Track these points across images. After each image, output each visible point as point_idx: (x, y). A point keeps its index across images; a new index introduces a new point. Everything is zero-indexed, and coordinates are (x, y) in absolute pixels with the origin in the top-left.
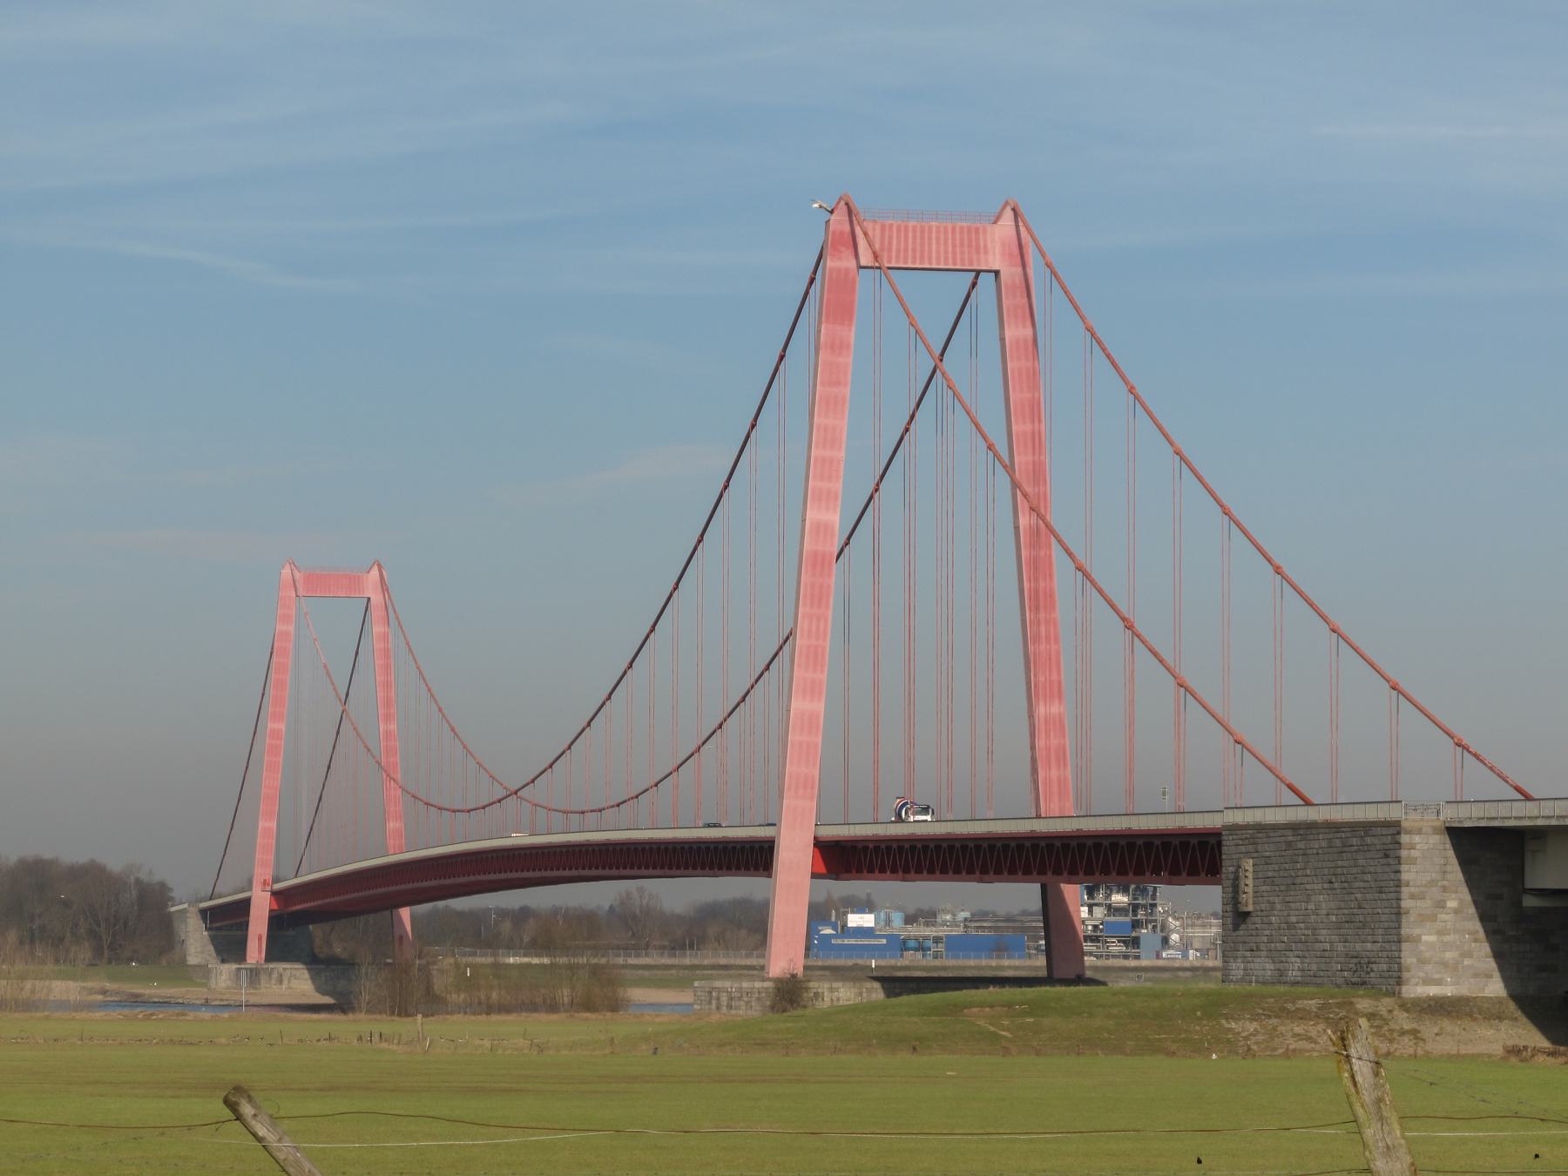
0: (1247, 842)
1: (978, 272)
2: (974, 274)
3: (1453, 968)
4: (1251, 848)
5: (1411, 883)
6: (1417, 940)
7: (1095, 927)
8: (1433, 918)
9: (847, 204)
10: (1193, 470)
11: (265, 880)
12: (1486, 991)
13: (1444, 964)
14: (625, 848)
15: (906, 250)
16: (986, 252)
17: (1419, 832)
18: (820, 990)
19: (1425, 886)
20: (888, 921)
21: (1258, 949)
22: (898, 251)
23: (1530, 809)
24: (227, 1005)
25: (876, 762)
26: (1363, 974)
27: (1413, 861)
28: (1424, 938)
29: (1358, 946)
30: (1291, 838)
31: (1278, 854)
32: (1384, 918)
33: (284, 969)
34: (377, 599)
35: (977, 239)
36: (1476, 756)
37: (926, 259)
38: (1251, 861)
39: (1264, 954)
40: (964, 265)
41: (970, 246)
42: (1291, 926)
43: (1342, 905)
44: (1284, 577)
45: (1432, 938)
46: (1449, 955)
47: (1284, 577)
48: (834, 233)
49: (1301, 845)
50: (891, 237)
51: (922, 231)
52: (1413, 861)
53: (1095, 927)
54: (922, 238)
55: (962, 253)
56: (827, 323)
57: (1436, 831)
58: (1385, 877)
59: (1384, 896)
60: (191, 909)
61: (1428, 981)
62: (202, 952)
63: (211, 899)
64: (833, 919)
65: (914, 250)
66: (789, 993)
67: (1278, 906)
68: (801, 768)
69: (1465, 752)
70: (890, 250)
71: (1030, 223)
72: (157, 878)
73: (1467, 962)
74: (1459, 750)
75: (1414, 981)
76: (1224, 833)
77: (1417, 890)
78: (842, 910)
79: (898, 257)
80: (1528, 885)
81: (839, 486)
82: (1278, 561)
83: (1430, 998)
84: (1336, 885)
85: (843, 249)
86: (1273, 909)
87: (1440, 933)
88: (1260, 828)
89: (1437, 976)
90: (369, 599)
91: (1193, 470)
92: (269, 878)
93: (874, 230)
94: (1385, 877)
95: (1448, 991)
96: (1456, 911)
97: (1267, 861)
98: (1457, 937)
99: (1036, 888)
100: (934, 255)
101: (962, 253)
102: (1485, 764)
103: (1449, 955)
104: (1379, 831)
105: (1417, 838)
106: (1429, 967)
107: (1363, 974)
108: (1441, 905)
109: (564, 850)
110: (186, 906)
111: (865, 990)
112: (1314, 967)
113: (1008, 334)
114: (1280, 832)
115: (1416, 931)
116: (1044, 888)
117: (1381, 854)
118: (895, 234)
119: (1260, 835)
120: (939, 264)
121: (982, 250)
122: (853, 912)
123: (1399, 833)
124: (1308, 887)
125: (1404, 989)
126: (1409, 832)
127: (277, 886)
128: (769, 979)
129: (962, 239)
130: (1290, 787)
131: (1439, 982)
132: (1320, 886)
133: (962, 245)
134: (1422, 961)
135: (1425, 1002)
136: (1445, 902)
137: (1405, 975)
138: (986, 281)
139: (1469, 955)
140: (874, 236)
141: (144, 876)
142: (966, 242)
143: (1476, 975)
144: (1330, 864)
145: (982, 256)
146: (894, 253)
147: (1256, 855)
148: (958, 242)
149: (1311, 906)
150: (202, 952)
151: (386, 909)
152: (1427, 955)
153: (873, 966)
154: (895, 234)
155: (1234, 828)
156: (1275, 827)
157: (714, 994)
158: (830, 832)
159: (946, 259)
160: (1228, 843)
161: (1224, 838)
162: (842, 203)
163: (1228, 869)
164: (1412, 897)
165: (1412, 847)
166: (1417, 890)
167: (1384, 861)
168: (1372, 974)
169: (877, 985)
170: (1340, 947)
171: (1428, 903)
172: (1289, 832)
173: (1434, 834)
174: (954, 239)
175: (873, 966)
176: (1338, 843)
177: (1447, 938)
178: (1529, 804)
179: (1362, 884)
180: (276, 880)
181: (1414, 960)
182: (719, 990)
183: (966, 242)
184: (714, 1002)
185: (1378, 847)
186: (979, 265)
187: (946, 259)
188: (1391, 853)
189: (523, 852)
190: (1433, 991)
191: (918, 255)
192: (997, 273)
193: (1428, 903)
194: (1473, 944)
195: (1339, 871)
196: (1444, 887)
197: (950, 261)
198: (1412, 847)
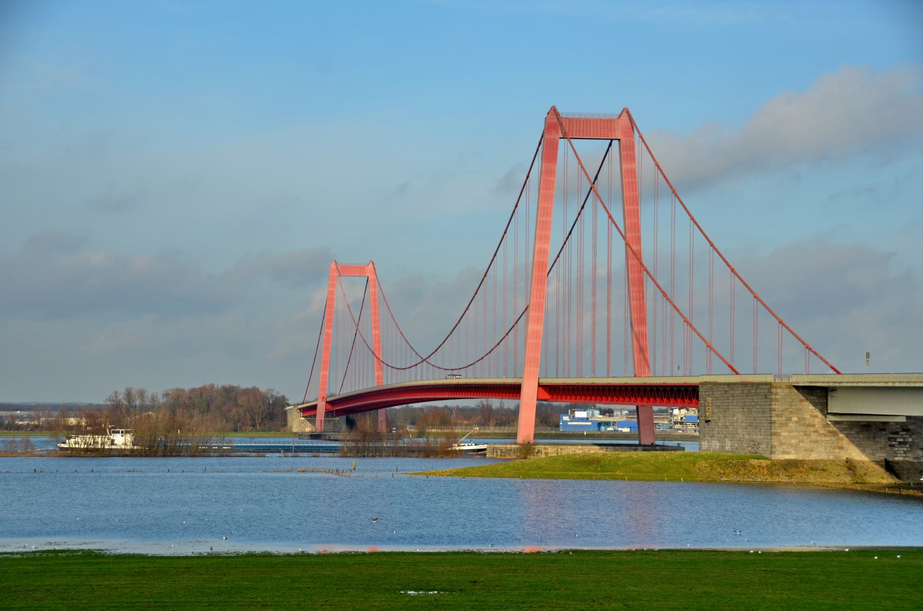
0: (709, 390)
1: (612, 140)
2: (610, 141)
3: (796, 447)
4: (711, 393)
5: (776, 410)
6: (778, 435)
7: (682, 418)
8: (786, 425)
9: (554, 110)
10: (699, 227)
11: (323, 397)
12: (810, 457)
13: (792, 445)
14: (462, 386)
15: (580, 130)
16: (614, 131)
17: (780, 388)
18: (540, 449)
19: (782, 411)
20: (593, 415)
21: (713, 436)
22: (576, 131)
23: (838, 378)
26: (756, 449)
28: (782, 434)
29: (754, 437)
30: (726, 389)
31: (721, 395)
32: (765, 425)
33: (332, 435)
34: (371, 277)
35: (611, 126)
36: (815, 353)
37: (578, 134)
38: (710, 399)
39: (716, 439)
40: (593, 136)
42: (726, 427)
43: (748, 418)
44: (736, 274)
45: (786, 434)
46: (793, 441)
47: (736, 274)
48: (548, 123)
49: (731, 392)
50: (573, 125)
52: (777, 400)
53: (682, 418)
54: (587, 125)
55: (604, 131)
56: (545, 162)
58: (766, 407)
59: (764, 415)
60: (295, 409)
61: (784, 453)
62: (299, 427)
63: (303, 404)
64: (569, 413)
65: (583, 131)
66: (527, 449)
67: (722, 418)
69: (810, 351)
70: (573, 131)
72: (280, 395)
73: (801, 444)
74: (807, 350)
75: (777, 452)
76: (700, 386)
77: (779, 412)
78: (573, 410)
79: (576, 133)
80: (829, 412)
82: (733, 266)
83: (786, 460)
84: (745, 410)
85: (552, 130)
86: (719, 419)
87: (789, 432)
88: (715, 384)
89: (789, 450)
90: (368, 277)
91: (699, 227)
93: (566, 122)
94: (766, 407)
95: (792, 457)
96: (796, 422)
97: (717, 399)
98: (797, 433)
100: (592, 132)
101: (604, 131)
103: (793, 441)
104: (763, 387)
105: (779, 390)
106: (784, 447)
107: (756, 449)
108: (789, 419)
109: (441, 387)
110: (292, 407)
111: (559, 449)
112: (736, 445)
113: (624, 167)
114: (722, 386)
115: (779, 431)
117: (764, 397)
118: (575, 123)
119: (714, 387)
120: (583, 136)
121: (613, 130)
122: (577, 411)
123: (771, 388)
124: (734, 410)
126: (776, 388)
128: (519, 444)
129: (604, 126)
131: (788, 453)
132: (739, 410)
133: (604, 128)
134: (781, 444)
135: (782, 461)
136: (791, 418)
138: (615, 143)
139: (803, 441)
140: (566, 124)
141: (275, 393)
142: (606, 127)
143: (806, 450)
144: (743, 401)
145: (613, 133)
146: (574, 132)
147: (712, 396)
148: (602, 127)
149: (735, 419)
150: (299, 427)
151: (374, 409)
152: (784, 441)
153: (585, 434)
154: (575, 123)
155: (706, 383)
156: (721, 384)
157: (495, 450)
158: (545, 381)
159: (597, 134)
160: (701, 390)
161: (700, 388)
163: (701, 401)
164: (777, 416)
165: (777, 394)
166: (779, 412)
167: (765, 400)
168: (760, 449)
170: (747, 437)
171: (784, 419)
172: (726, 386)
173: (786, 388)
174: (600, 126)
175: (585, 434)
176: (746, 392)
177: (792, 434)
178: (839, 376)
179: (756, 410)
181: (778, 443)
182: (497, 449)
183: (606, 127)
184: (495, 454)
185: (762, 394)
186: (611, 137)
187: (597, 134)
188: (768, 397)
189: (429, 387)
190: (787, 457)
191: (585, 132)
192: (619, 140)
193: (784, 419)
194: (804, 437)
195: (746, 404)
196: (791, 412)
197: (599, 135)
198: (777, 394)
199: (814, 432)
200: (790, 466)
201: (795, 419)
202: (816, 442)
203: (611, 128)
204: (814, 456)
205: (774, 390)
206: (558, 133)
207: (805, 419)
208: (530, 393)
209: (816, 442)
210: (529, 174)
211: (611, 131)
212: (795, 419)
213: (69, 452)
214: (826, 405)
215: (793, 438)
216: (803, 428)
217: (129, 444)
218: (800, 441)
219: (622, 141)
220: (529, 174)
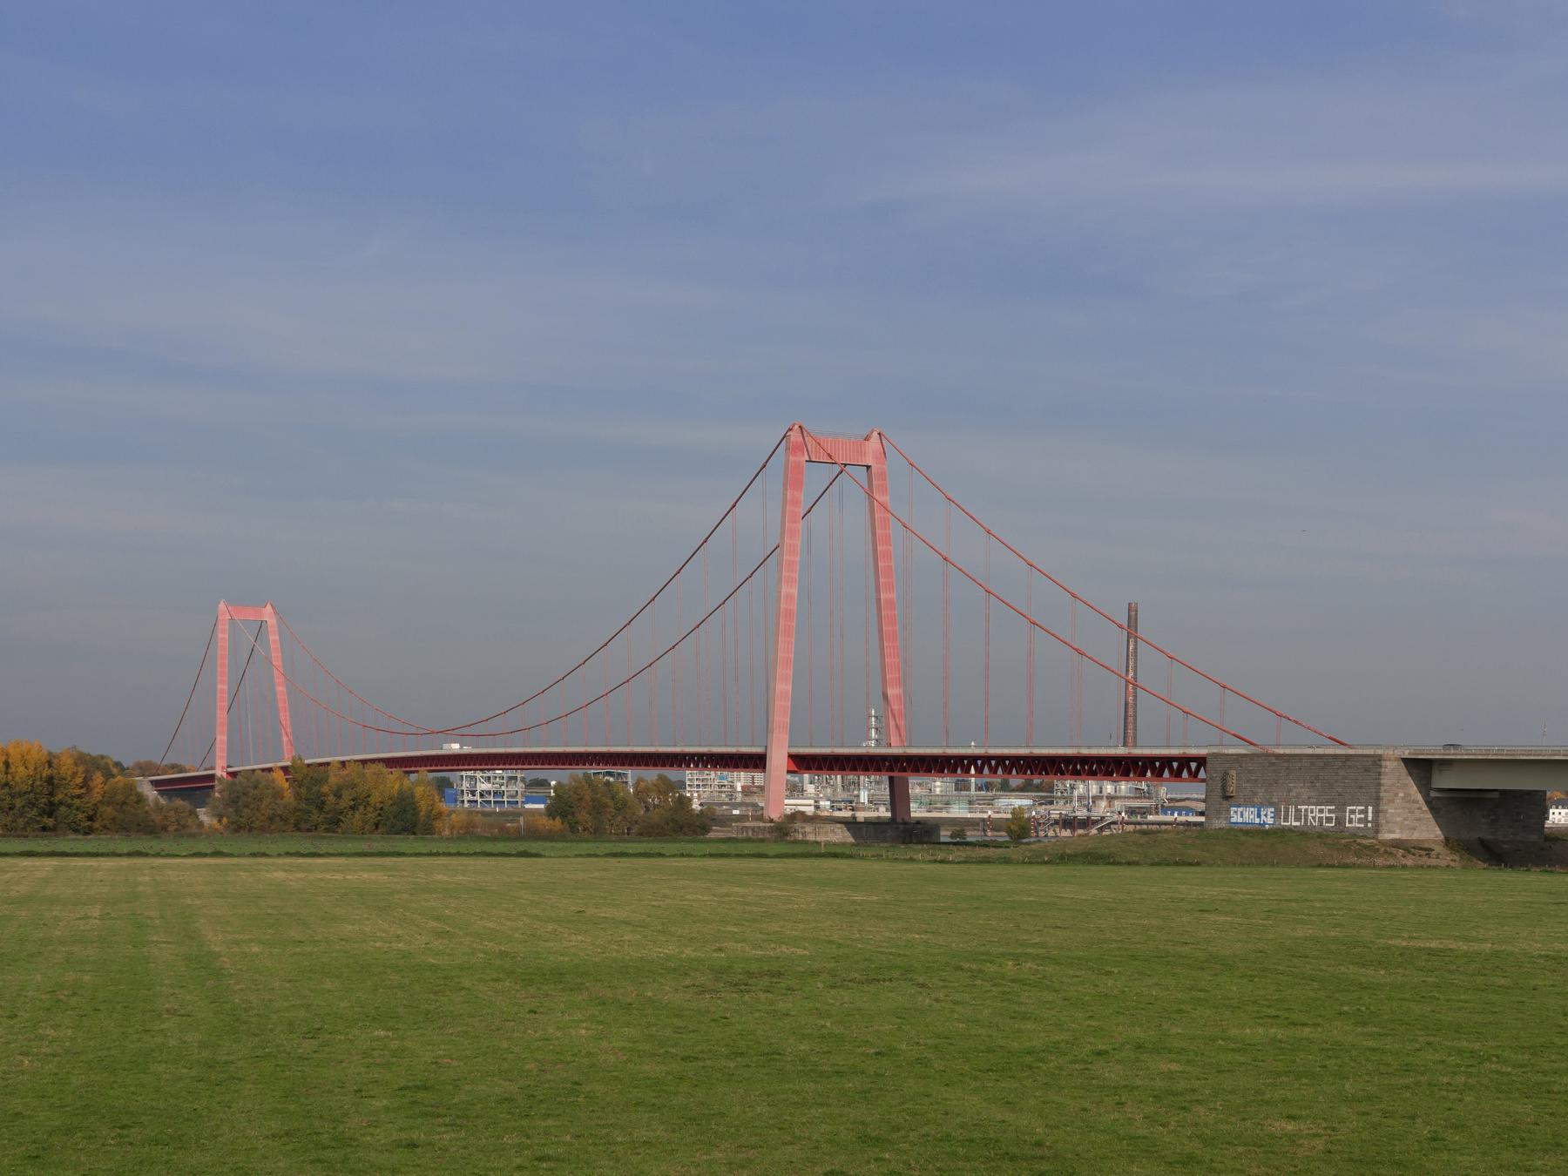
6: (1386, 812)
13: (1396, 823)
16: (865, 456)
17: (1390, 760)
24: (1163, 824)
25: (987, 717)
27: (1385, 773)
28: (1390, 811)
41: (857, 452)
45: (1393, 811)
46: (1398, 819)
51: (835, 443)
57: (1396, 759)
61: (1390, 832)
68: (781, 718)
71: (888, 436)
73: (1406, 822)
81: (797, 575)
92: (225, 766)
96: (1403, 798)
99: (885, 778)
102: (1304, 726)
105: (1388, 763)
108: (1396, 795)
116: (891, 779)
125: (1380, 835)
127: (230, 770)
130: (1234, 735)
131: (1393, 832)
137: (1381, 828)
158: (795, 751)
162: (796, 427)
164: (1385, 791)
169: (843, 826)
171: (1391, 794)
177: (1398, 811)
180: (229, 767)
192: (868, 467)
193: (1391, 794)
198: (1386, 767)
199: (1418, 809)
200: (1397, 844)
201: (1401, 795)
202: (1419, 820)
203: (861, 452)
204: (1416, 836)
205: (1383, 763)
206: (803, 454)
207: (1410, 795)
208: (778, 760)
209: (1419, 820)
210: (707, 538)
211: (861, 455)
212: (1401, 795)
213: (642, 812)
214: (1429, 779)
215: (1399, 815)
216: (1408, 805)
217: (104, 761)
218: (1405, 819)
219: (874, 469)
220: (707, 538)
